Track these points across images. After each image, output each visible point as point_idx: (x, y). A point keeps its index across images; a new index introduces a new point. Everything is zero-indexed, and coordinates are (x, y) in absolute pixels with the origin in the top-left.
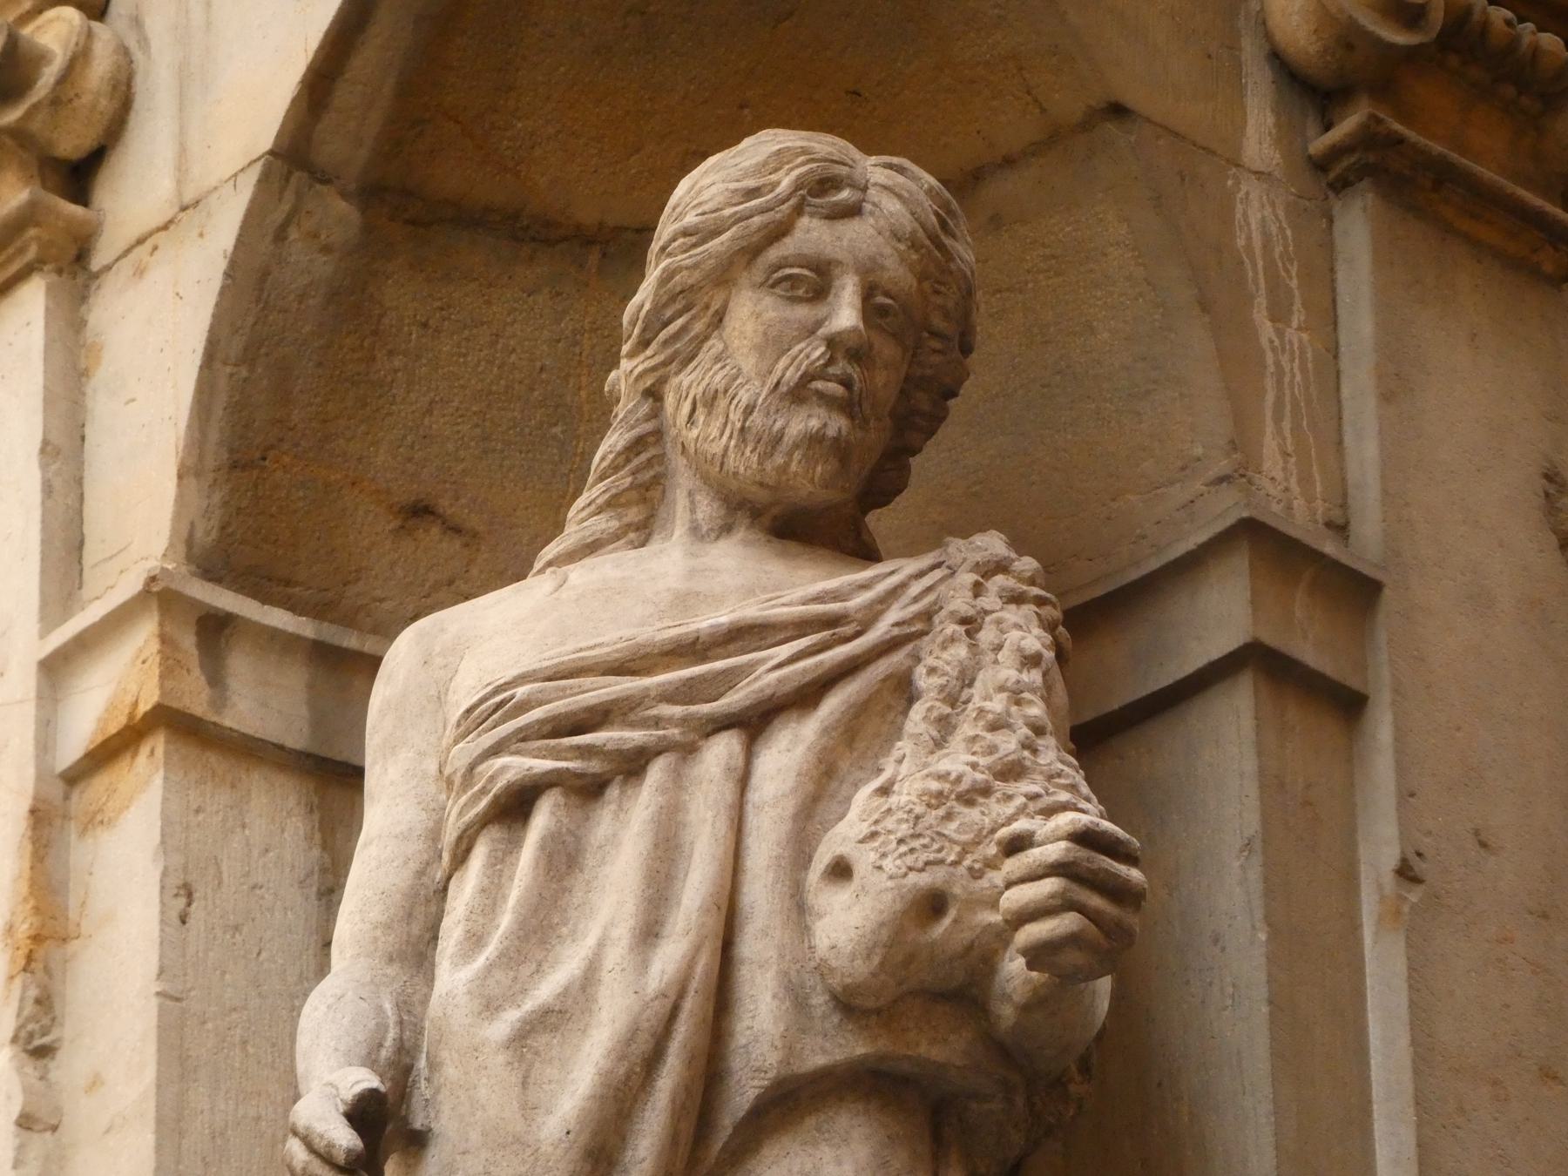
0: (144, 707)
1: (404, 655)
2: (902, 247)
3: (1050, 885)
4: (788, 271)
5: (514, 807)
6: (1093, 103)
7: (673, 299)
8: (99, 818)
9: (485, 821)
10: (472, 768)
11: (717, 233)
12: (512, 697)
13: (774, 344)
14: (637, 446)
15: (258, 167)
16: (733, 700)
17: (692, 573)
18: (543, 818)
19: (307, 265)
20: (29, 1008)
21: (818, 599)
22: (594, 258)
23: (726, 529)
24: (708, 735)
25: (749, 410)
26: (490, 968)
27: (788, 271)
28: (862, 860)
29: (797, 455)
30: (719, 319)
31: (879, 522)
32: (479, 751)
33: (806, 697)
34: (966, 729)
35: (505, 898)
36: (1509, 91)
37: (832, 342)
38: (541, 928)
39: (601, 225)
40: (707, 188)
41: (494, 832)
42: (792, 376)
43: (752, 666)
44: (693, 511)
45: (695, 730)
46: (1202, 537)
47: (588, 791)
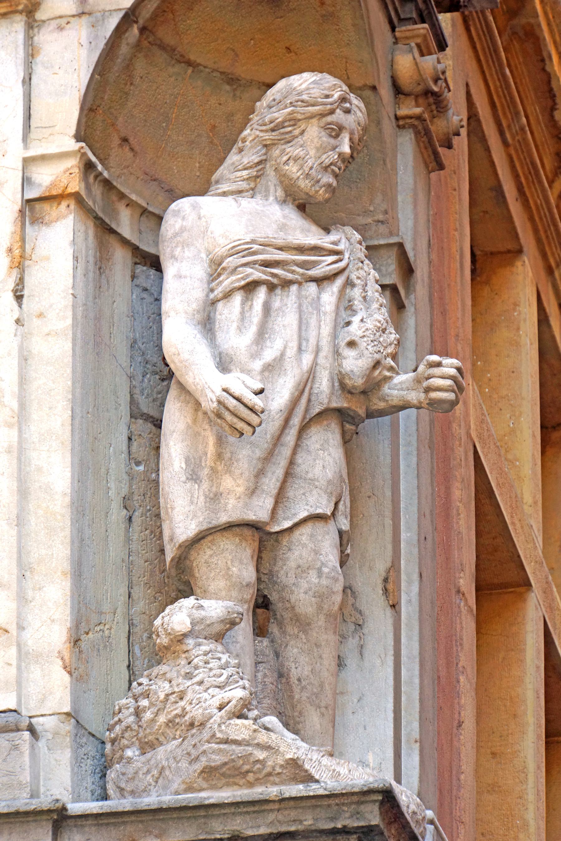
2: (359, 128)
3: (449, 382)
4: (333, 126)
5: (250, 287)
6: (368, 83)
7: (289, 120)
8: (40, 220)
10: (237, 268)
11: (313, 105)
12: (251, 248)
13: (322, 149)
15: (121, 14)
16: (315, 272)
18: (262, 293)
20: (18, 281)
24: (307, 281)
25: (311, 168)
27: (333, 126)
28: (363, 344)
29: (323, 189)
32: (240, 263)
37: (340, 154)
39: (195, 61)
42: (327, 162)
44: (276, 192)
45: (304, 279)
47: (272, 288)
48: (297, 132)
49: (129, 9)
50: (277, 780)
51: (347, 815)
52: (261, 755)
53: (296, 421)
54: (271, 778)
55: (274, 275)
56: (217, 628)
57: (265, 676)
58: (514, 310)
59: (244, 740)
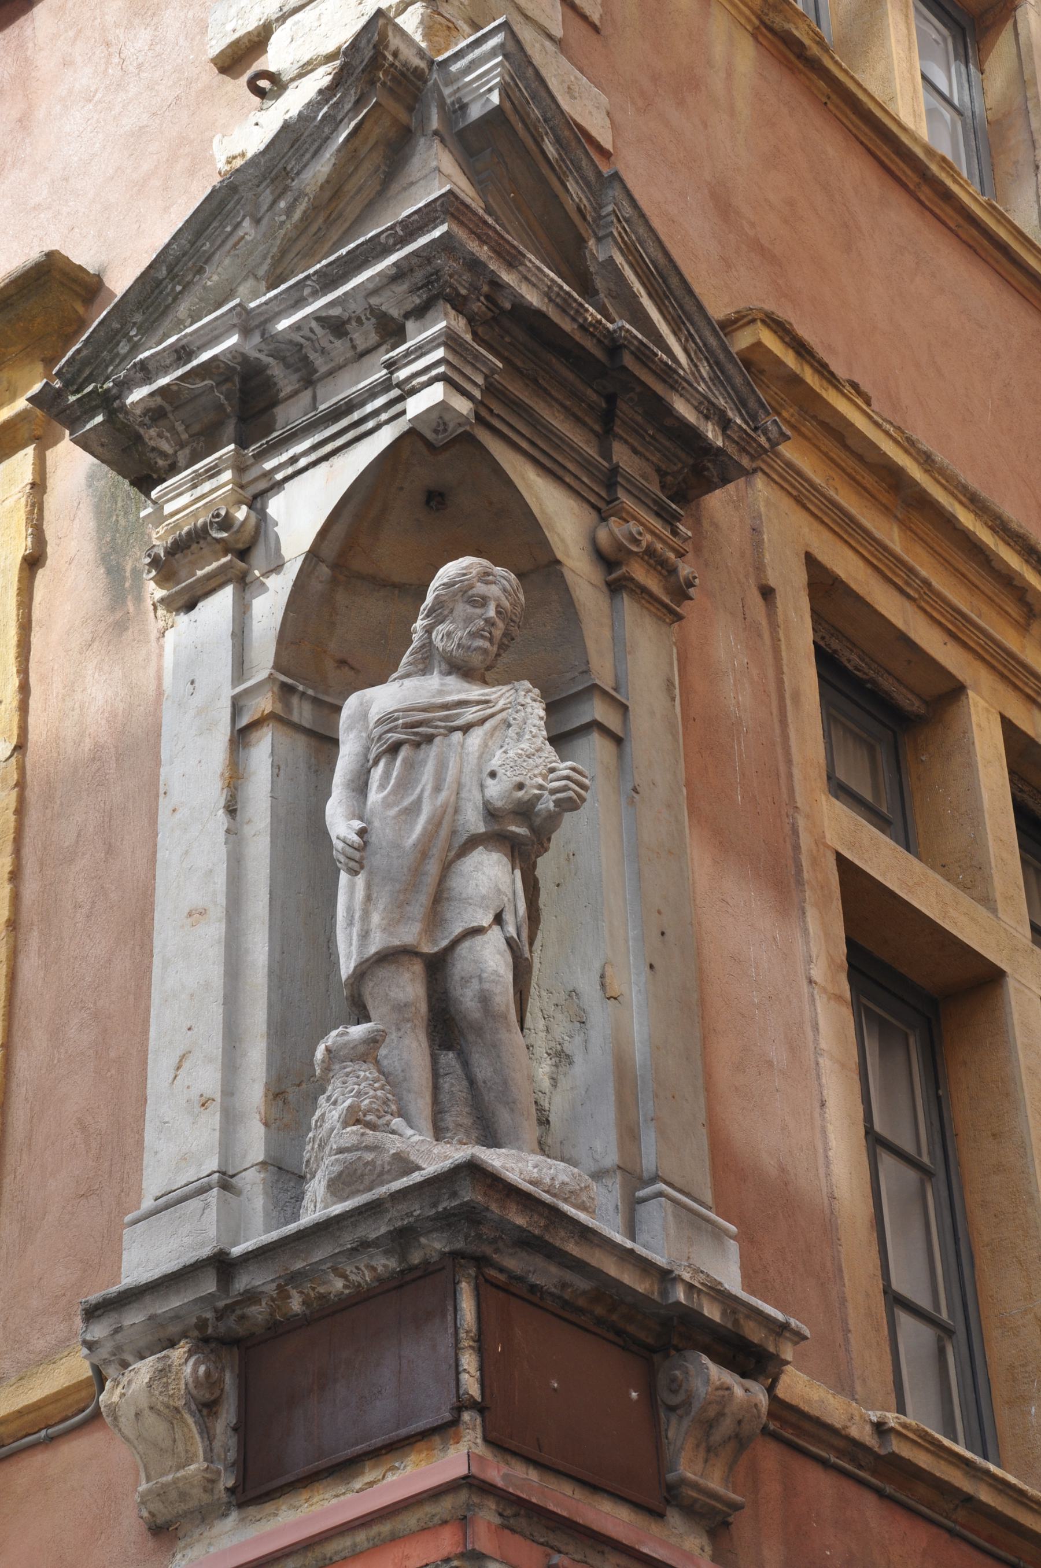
0: (266, 712)
1: (352, 704)
5: (394, 749)
9: (385, 752)
14: (423, 646)
15: (303, 556)
17: (442, 685)
18: (404, 752)
19: (316, 586)
20: (229, 798)
21: (482, 695)
22: (396, 592)
23: (449, 674)
25: (461, 638)
26: (389, 794)
28: (500, 772)
30: (452, 611)
31: (489, 675)
33: (482, 721)
34: (527, 736)
35: (391, 775)
36: (659, 568)
38: (405, 784)
40: (449, 570)
41: (388, 755)
43: (465, 713)
46: (580, 688)
47: (417, 745)
48: (446, 612)
49: (309, 552)
50: (390, 1178)
51: (446, 1197)
52: (369, 1156)
53: (436, 852)
54: (385, 1177)
55: (416, 734)
56: (362, 1049)
57: (452, 1085)
58: (964, 737)
59: (353, 1145)
